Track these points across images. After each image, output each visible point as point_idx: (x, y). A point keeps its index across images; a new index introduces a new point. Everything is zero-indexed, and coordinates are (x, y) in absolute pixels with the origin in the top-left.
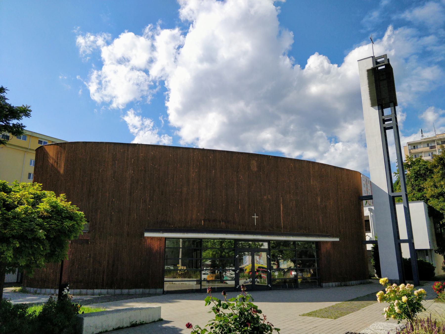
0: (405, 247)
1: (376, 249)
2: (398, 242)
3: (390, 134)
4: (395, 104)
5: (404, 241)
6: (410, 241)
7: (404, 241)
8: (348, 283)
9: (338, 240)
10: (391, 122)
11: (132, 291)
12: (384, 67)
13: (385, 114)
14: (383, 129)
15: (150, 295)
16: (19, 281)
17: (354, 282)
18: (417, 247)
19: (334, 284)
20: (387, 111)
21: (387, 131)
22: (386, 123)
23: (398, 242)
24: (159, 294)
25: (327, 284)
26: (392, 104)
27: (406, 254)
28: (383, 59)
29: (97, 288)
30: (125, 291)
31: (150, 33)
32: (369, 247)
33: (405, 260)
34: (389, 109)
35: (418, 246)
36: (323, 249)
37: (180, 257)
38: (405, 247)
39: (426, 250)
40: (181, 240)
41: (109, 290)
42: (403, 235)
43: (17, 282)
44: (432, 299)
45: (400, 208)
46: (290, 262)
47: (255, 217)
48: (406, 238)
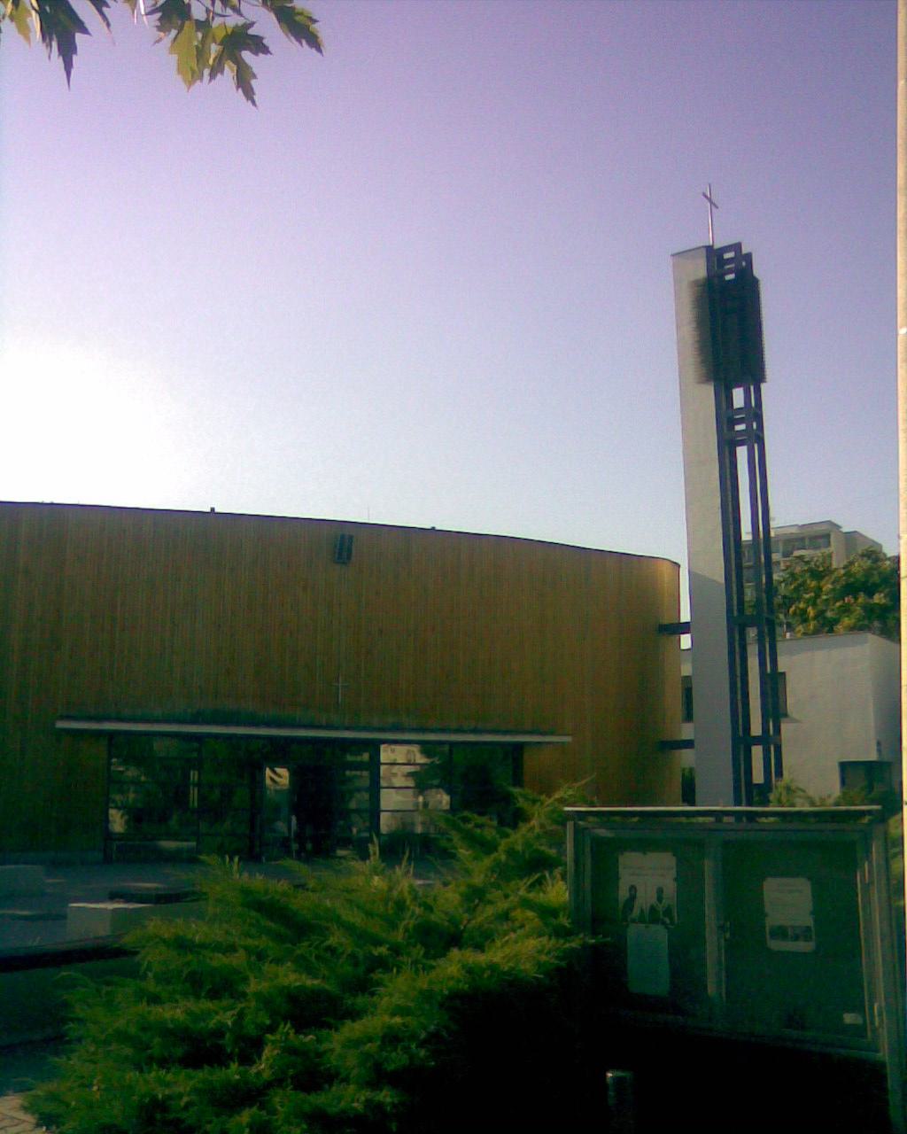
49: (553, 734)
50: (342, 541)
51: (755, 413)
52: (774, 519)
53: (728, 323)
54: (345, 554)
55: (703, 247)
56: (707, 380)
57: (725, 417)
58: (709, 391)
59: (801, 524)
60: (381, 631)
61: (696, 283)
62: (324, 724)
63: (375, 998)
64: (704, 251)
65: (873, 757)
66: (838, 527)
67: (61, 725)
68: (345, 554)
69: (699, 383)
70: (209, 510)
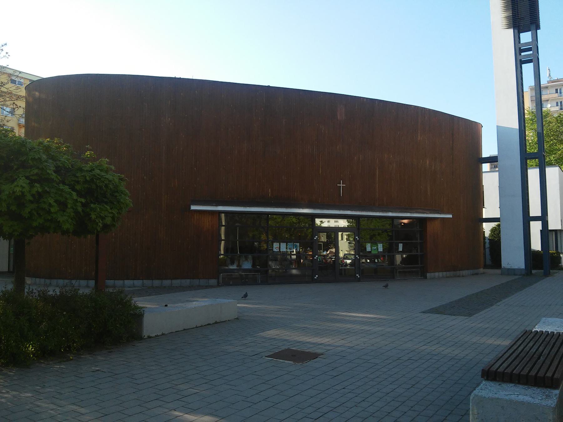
0: (536, 227)
1: (496, 232)
3: (528, 69)
4: (538, 27)
5: (536, 219)
6: (543, 218)
7: (536, 219)
8: (458, 273)
9: (450, 216)
10: (531, 52)
11: (176, 282)
13: (523, 41)
14: (518, 62)
16: (11, 270)
17: (465, 272)
19: (441, 274)
20: (526, 37)
21: (523, 65)
22: (523, 54)
23: (527, 219)
24: (212, 287)
25: (432, 274)
26: (533, 27)
27: (536, 245)
29: (128, 279)
30: (167, 282)
32: (487, 228)
33: (536, 253)
34: (529, 33)
36: (430, 228)
38: (536, 227)
41: (145, 281)
42: (535, 210)
43: (9, 272)
44: (548, 236)
45: (533, 174)
47: (341, 185)
51: (534, 46)
57: (519, 49)
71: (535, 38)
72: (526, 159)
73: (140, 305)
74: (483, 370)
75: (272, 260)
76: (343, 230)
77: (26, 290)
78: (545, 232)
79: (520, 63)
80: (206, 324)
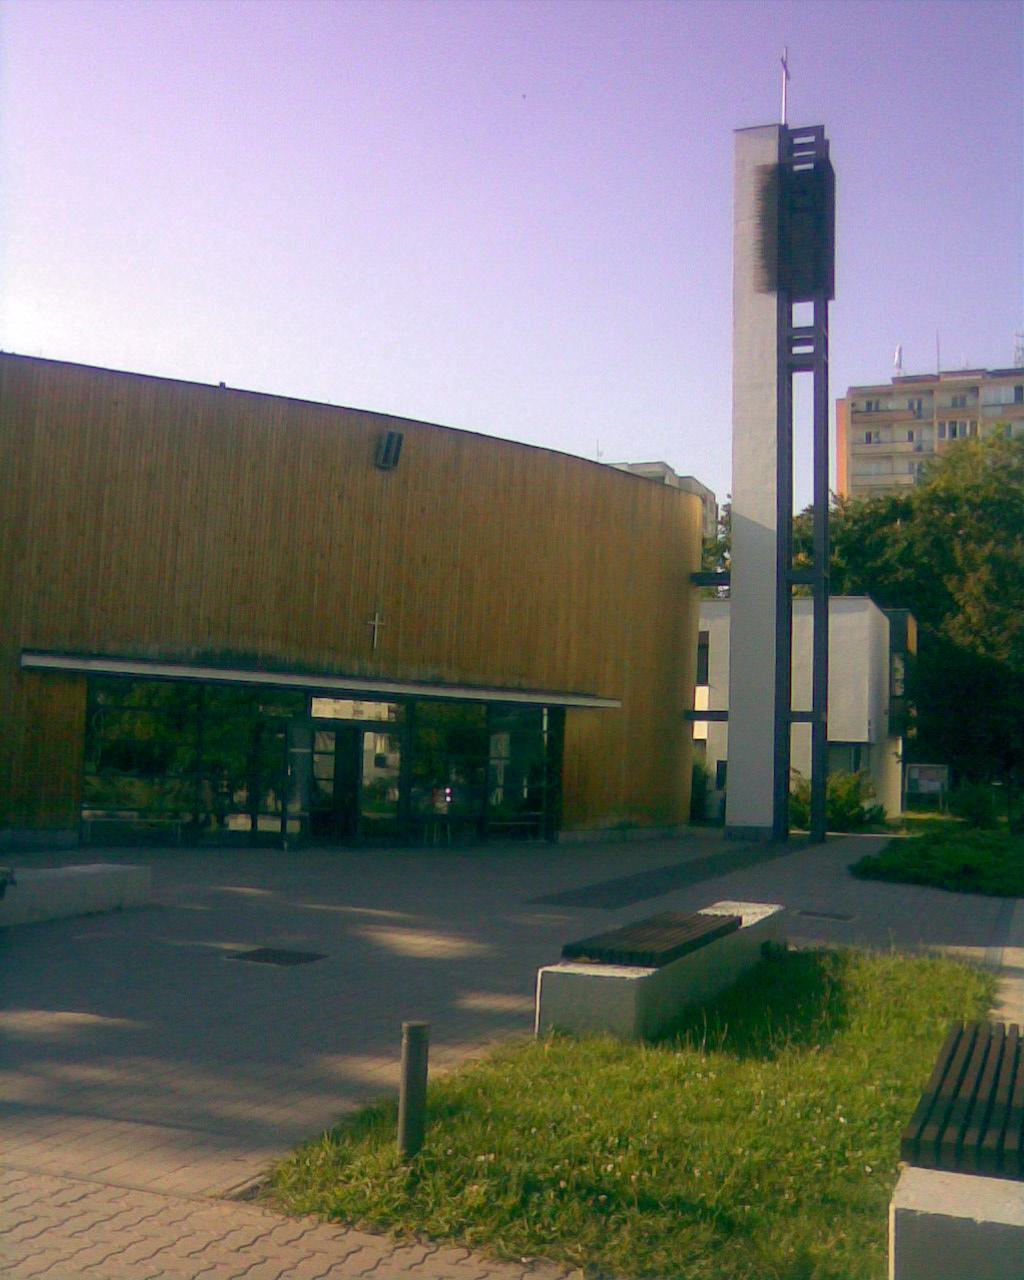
0: (801, 736)
2: (785, 717)
3: (803, 384)
5: (802, 717)
6: (818, 716)
7: (802, 717)
12: (810, 166)
13: (797, 322)
15: (459, 1044)
18: (835, 734)
20: (803, 314)
23: (785, 717)
28: (811, 139)
31: (965, 978)
35: (835, 734)
37: (545, 728)
38: (801, 736)
39: (858, 746)
40: (545, 711)
42: (802, 698)
46: (643, 1053)
48: (808, 707)
49: (594, 696)
50: (389, 441)
51: (819, 334)
52: (600, 454)
53: (796, 226)
54: (392, 454)
55: (774, 125)
56: (769, 290)
57: (787, 336)
58: (772, 301)
59: (630, 462)
60: (424, 560)
61: (763, 170)
62: (356, 673)
63: (993, 1033)
64: (776, 131)
65: (864, 738)
66: (672, 471)
67: (29, 661)
68: (392, 454)
69: (760, 291)
70: (217, 383)
71: (822, 316)
72: (790, 583)
73: (482, 946)
74: (904, 1140)
75: (275, 790)
76: (377, 726)
77: (918, 1100)
78: (824, 749)
79: (788, 366)
80: (1019, 1073)
